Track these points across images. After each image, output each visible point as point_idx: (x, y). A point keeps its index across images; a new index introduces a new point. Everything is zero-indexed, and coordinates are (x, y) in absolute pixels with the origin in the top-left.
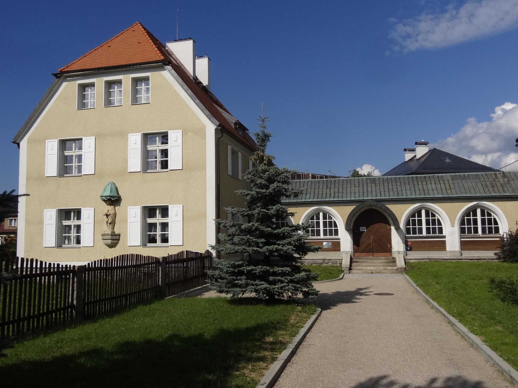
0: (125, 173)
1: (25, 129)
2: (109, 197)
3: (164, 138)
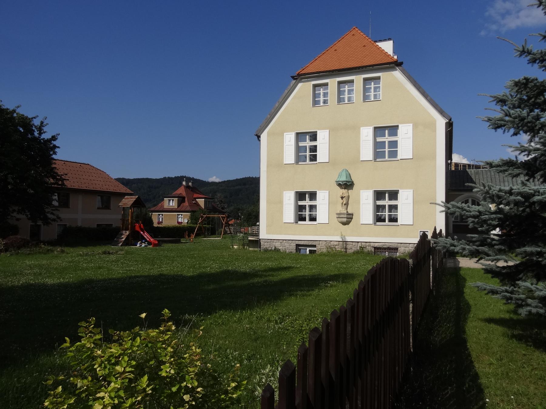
0: (357, 161)
1: (266, 123)
2: (345, 182)
3: (314, 136)
